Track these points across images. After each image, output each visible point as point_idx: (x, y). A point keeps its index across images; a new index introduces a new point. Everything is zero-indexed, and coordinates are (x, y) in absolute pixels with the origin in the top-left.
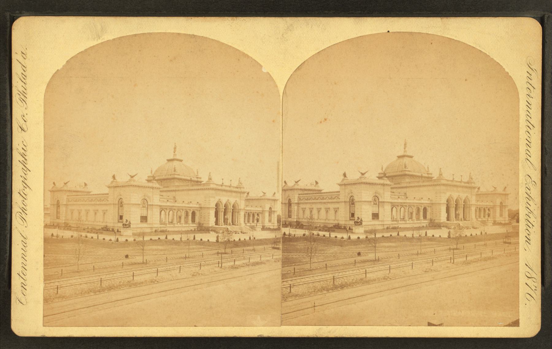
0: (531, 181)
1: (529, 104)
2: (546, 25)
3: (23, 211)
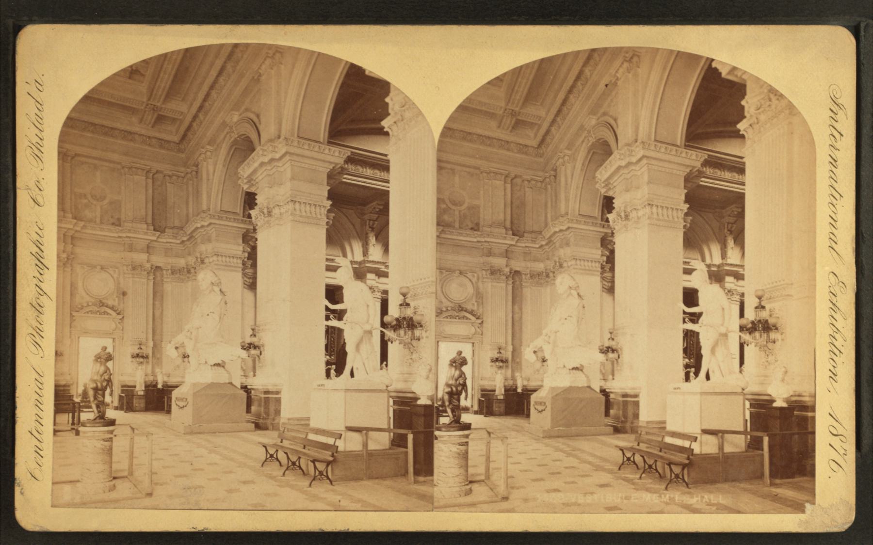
0: (837, 281)
1: (834, 162)
2: (862, 39)
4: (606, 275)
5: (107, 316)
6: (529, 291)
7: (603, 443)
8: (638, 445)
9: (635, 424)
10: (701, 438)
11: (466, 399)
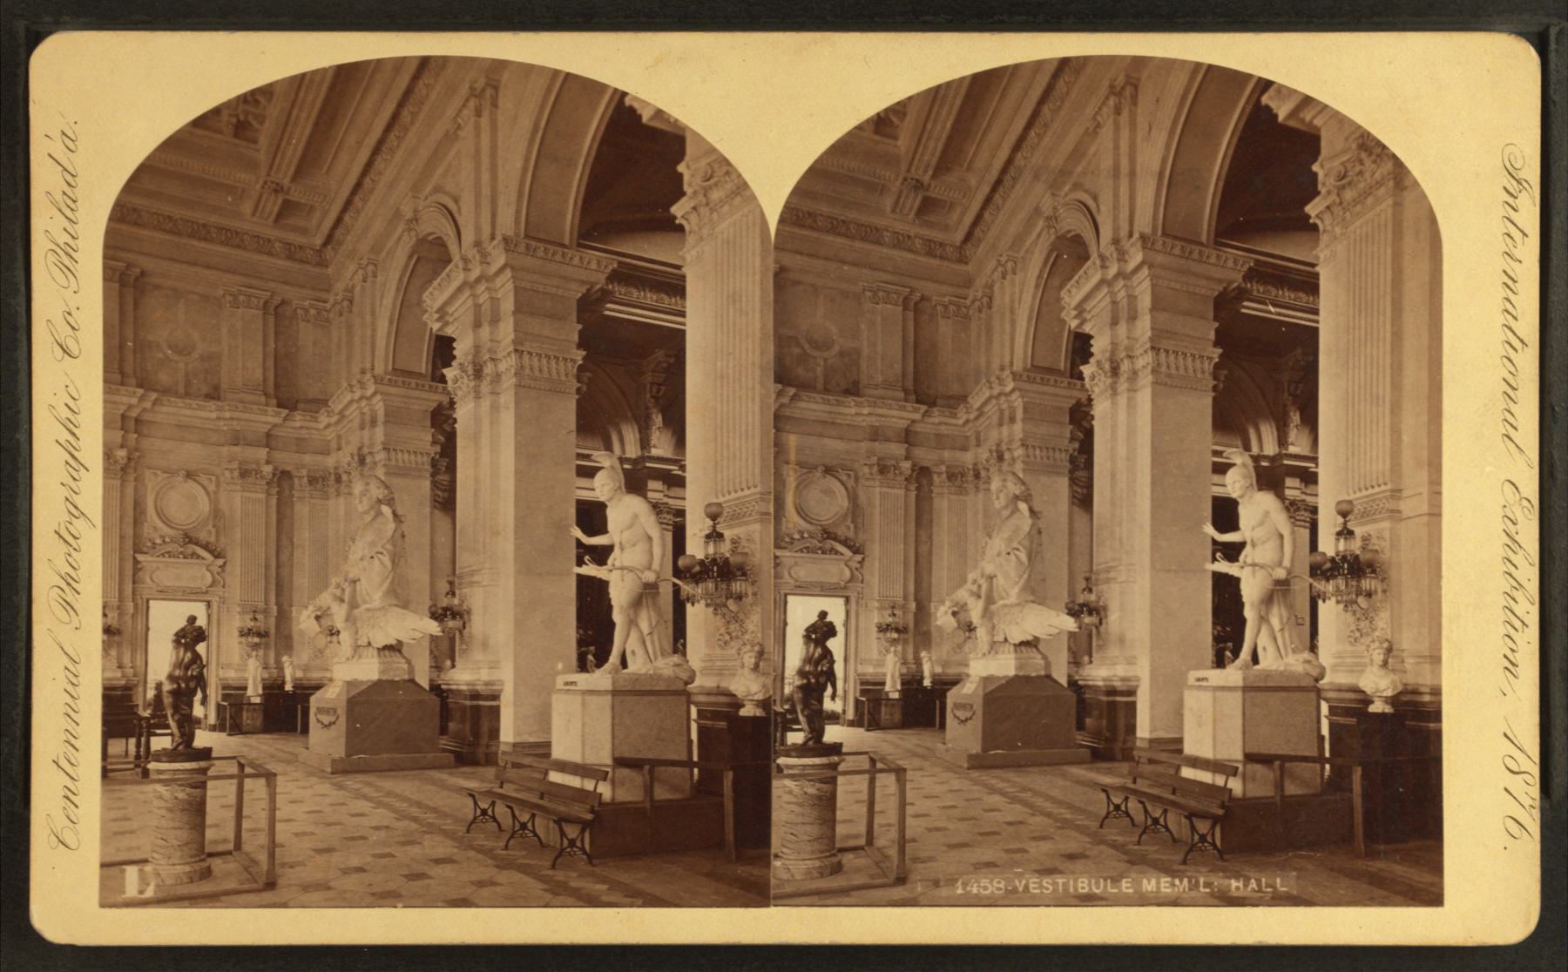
2: (1553, 57)
3: (69, 584)
4: (440, 477)
5: (835, 557)
6: (944, 503)
7: (443, 786)
8: (1134, 782)
9: (1129, 744)
10: (614, 772)
11: (833, 697)
